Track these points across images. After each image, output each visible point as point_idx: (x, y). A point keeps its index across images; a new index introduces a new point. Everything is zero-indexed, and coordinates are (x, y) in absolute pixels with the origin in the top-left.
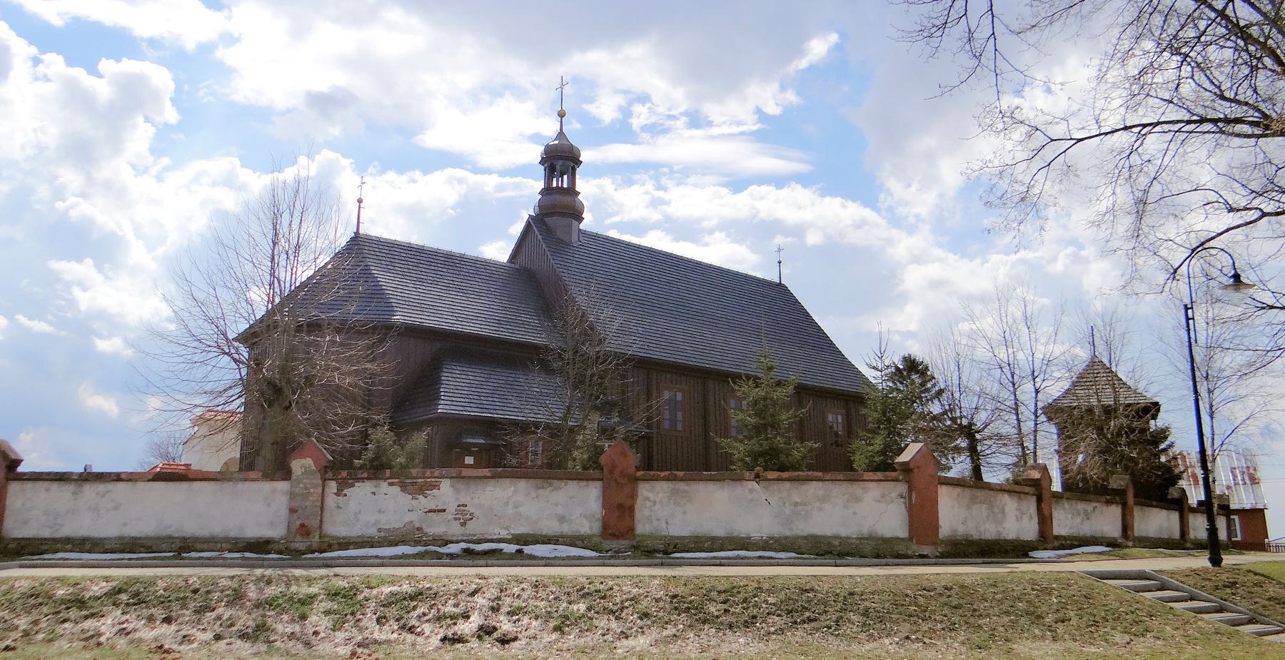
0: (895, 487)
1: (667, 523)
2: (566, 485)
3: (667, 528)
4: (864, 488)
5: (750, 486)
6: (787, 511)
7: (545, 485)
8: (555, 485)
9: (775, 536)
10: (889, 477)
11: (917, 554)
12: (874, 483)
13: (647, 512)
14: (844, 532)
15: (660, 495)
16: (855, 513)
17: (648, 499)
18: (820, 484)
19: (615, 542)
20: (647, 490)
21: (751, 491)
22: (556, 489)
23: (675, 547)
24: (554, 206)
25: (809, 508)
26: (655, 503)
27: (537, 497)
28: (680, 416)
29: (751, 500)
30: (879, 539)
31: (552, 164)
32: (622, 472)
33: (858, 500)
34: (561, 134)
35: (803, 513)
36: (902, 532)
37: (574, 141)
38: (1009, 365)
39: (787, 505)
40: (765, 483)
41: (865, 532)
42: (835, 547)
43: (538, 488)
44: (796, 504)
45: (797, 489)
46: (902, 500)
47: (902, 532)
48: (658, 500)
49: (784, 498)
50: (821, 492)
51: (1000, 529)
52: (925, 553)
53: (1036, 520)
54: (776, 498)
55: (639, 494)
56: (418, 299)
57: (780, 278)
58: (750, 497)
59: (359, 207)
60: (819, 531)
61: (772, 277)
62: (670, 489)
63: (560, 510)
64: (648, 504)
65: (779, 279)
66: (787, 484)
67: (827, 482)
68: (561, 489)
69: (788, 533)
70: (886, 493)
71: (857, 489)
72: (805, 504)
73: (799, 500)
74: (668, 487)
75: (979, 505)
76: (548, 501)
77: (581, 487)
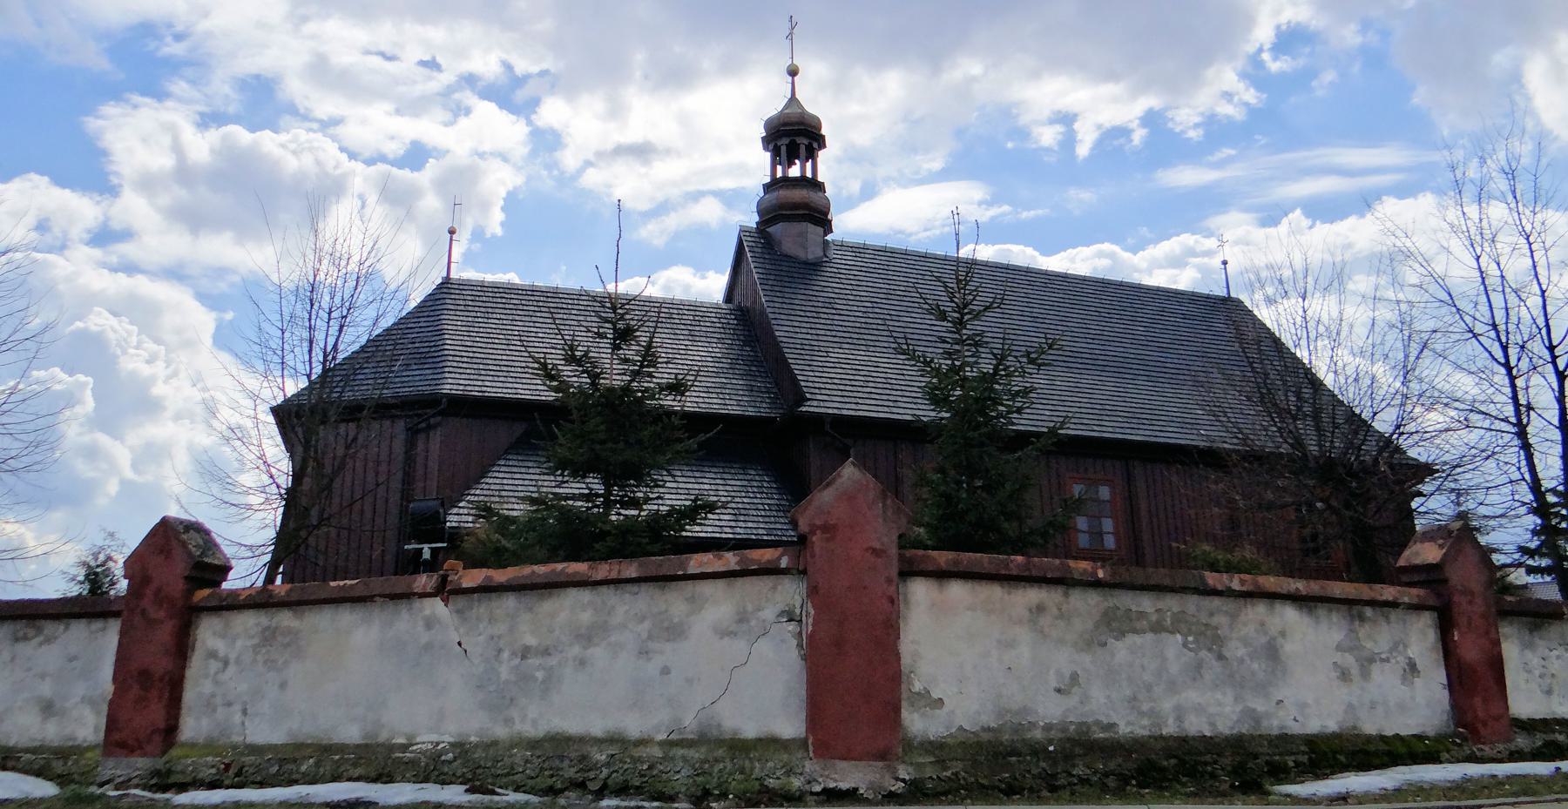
0: (774, 588)
1: (245, 712)
2: (67, 628)
3: (243, 723)
4: (692, 600)
5: (427, 612)
6: (504, 672)
7: (31, 632)
8: (46, 632)
9: (472, 739)
10: (753, 561)
11: (818, 788)
12: (720, 584)
13: (207, 687)
14: (633, 726)
15: (239, 643)
16: (666, 671)
17: (213, 655)
18: (585, 595)
19: (125, 761)
20: (214, 634)
21: (429, 624)
22: (48, 641)
23: (238, 774)
24: (782, 206)
25: (552, 661)
26: (226, 663)
27: (13, 659)
28: (1108, 525)
29: (428, 647)
30: (720, 742)
31: (776, 146)
32: (159, 590)
33: (674, 632)
34: (793, 99)
35: (540, 675)
36: (790, 726)
37: (811, 108)
38: (1495, 326)
39: (506, 655)
40: (461, 601)
41: (689, 722)
42: (596, 767)
43: (17, 640)
44: (525, 653)
45: (531, 610)
46: (792, 627)
47: (790, 726)
48: (233, 656)
49: (499, 637)
50: (586, 617)
51: (1260, 705)
52: (844, 786)
53: (189, 696)
54: (481, 638)
55: (198, 645)
56: (462, 357)
57: (1228, 287)
58: (425, 638)
59: (451, 240)
60: (572, 725)
61: (1220, 291)
62: (260, 629)
63: (46, 689)
64: (214, 666)
65: (1225, 290)
66: (510, 602)
67: (604, 589)
68: (56, 638)
69: (501, 732)
70: (750, 608)
71: (674, 601)
72: (546, 652)
73: (531, 641)
74: (257, 625)
75: (1149, 636)
76: (29, 669)
77: (92, 633)
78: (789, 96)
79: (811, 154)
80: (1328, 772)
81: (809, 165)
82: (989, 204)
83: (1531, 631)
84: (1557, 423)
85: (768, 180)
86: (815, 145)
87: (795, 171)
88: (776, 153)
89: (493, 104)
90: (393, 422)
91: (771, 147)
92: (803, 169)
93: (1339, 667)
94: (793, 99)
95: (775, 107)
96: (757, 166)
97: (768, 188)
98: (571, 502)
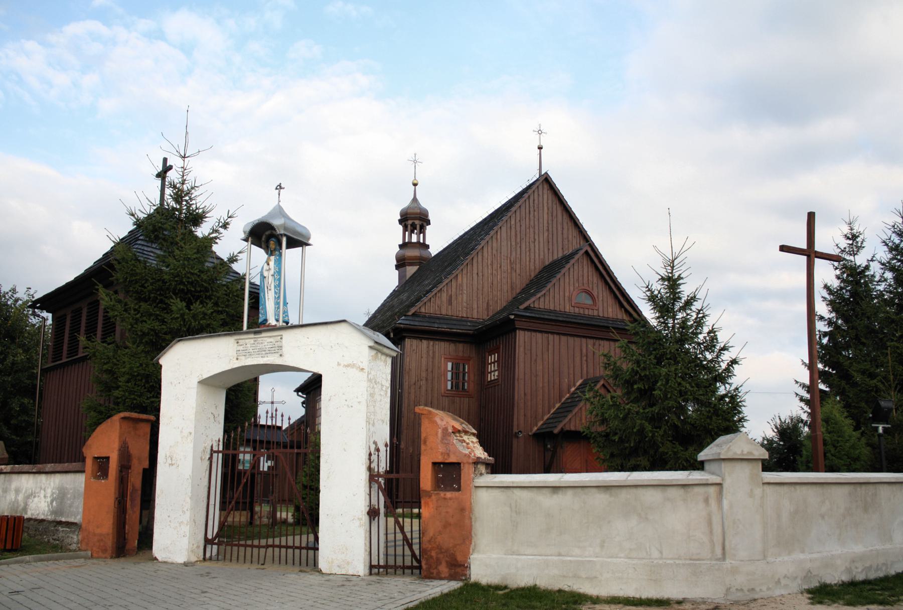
31: (405, 224)
34: (415, 199)
78: (413, 197)
79: (422, 230)
80: (138, 411)
81: (422, 235)
82: (652, 298)
83: (536, 585)
84: (292, 422)
85: (401, 243)
86: (425, 224)
87: (414, 239)
88: (405, 229)
89: (397, 284)
90: (377, 353)
91: (403, 224)
92: (419, 238)
93: (318, 571)
94: (415, 199)
95: (405, 203)
96: (396, 235)
97: (401, 246)
98: (550, 557)
